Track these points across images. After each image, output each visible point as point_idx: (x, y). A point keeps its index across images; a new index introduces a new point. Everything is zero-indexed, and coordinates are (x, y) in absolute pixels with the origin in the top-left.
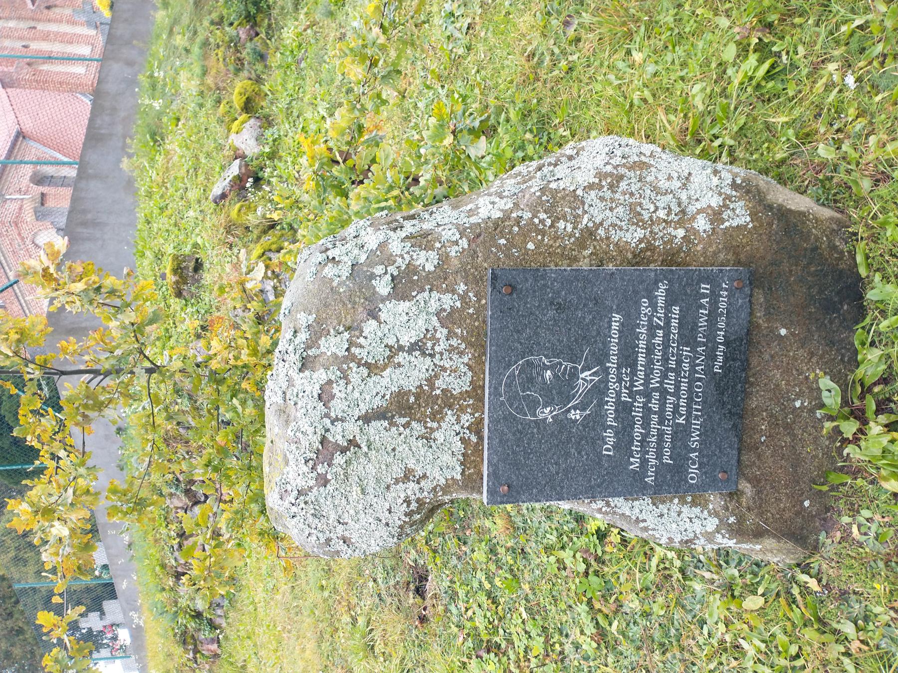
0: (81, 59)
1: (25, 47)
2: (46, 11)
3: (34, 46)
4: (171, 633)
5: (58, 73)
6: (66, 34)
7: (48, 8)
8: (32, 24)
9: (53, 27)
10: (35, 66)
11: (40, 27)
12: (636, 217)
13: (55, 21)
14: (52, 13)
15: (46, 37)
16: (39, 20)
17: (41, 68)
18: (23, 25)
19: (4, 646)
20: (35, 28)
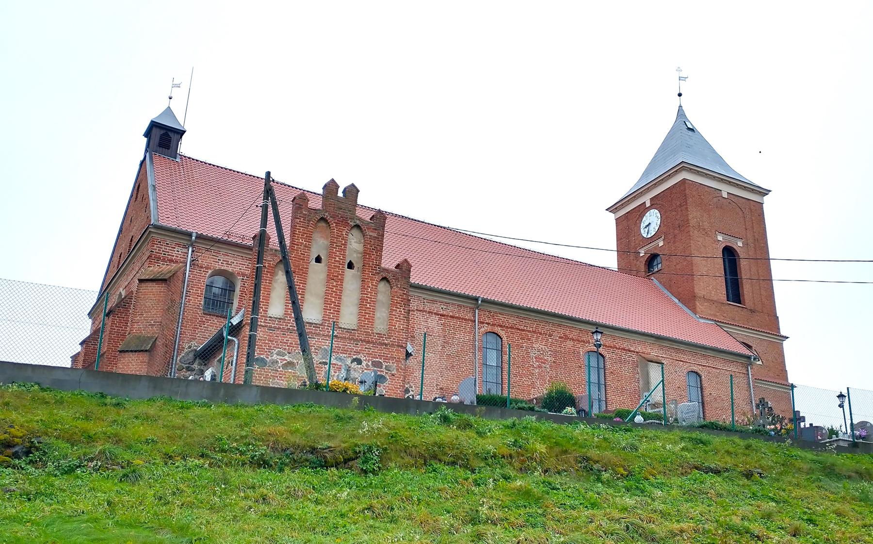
15: (334, 280)
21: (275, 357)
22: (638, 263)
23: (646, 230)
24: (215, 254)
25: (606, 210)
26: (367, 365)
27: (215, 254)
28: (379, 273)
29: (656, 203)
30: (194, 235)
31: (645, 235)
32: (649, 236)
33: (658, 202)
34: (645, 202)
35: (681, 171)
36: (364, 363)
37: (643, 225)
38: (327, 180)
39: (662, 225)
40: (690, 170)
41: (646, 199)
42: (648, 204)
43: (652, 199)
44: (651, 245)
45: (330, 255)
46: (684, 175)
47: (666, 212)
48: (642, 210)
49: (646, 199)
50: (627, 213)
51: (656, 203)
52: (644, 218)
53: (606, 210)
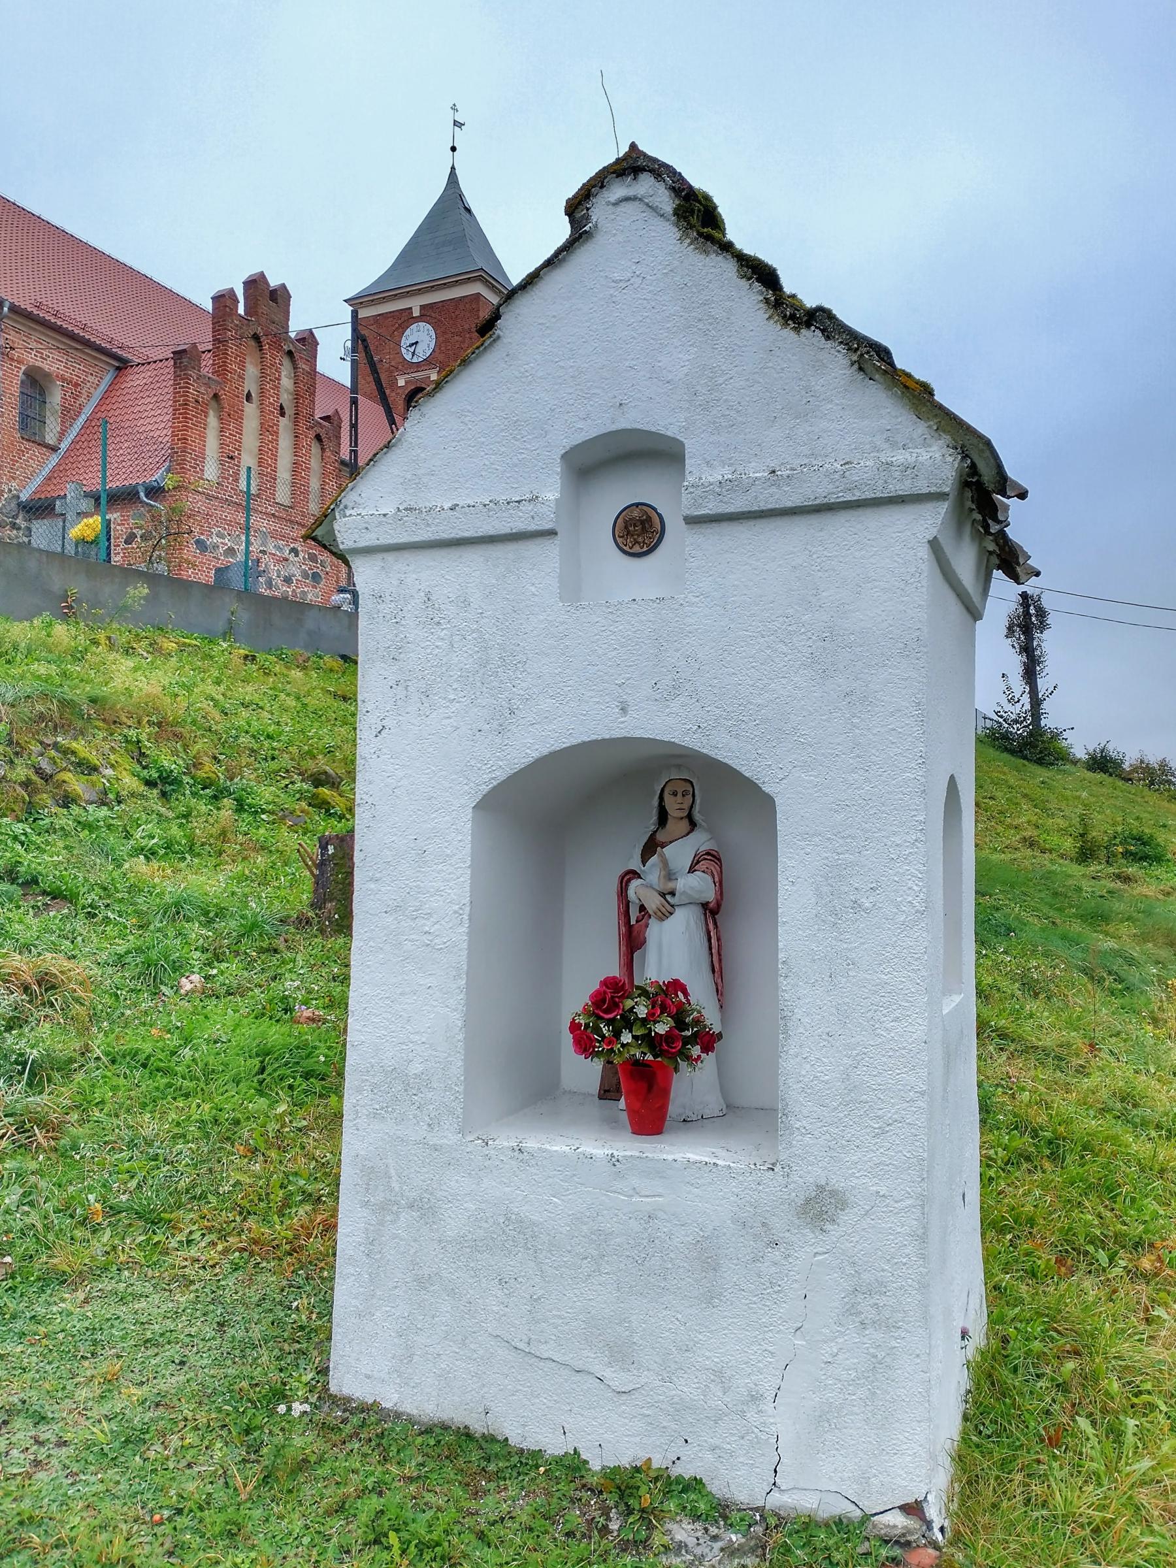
0: (249, 484)
1: (249, 397)
2: (312, 434)
3: (251, 411)
4: (422, 1413)
5: (203, 438)
6: (275, 457)
7: (318, 438)
8: (289, 411)
9: (285, 443)
10: (213, 404)
11: (284, 422)
12: (804, 1235)
13: (297, 447)
14: (308, 440)
15: (267, 430)
16: (296, 422)
17: (211, 413)
18: (286, 399)
19: (258, 1566)
20: (283, 414)
21: (215, 539)
22: (394, 394)
23: (412, 349)
24: (25, 339)
25: (345, 301)
26: (304, 558)
27: (25, 339)
28: (312, 428)
29: (428, 313)
30: (7, 304)
31: (408, 357)
32: (415, 360)
33: (433, 315)
34: (411, 308)
35: (475, 281)
36: (301, 555)
37: (405, 342)
38: (255, 270)
39: (437, 350)
40: (486, 283)
41: (415, 304)
42: (416, 313)
43: (423, 307)
44: (419, 374)
45: (262, 392)
46: (477, 288)
47: (444, 333)
48: (404, 319)
49: (415, 304)
50: (379, 315)
51: (428, 313)
52: (408, 332)
53: (345, 301)
